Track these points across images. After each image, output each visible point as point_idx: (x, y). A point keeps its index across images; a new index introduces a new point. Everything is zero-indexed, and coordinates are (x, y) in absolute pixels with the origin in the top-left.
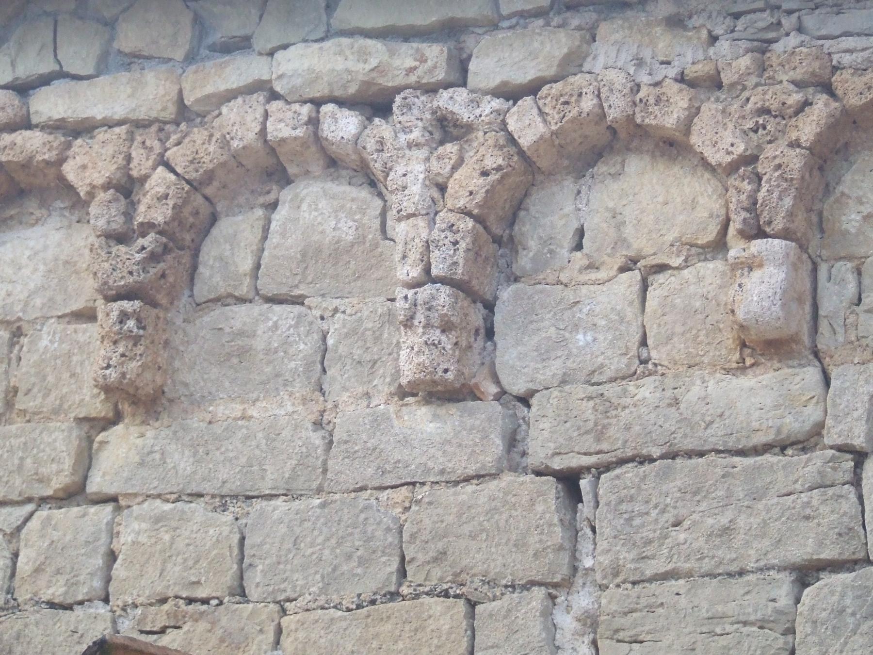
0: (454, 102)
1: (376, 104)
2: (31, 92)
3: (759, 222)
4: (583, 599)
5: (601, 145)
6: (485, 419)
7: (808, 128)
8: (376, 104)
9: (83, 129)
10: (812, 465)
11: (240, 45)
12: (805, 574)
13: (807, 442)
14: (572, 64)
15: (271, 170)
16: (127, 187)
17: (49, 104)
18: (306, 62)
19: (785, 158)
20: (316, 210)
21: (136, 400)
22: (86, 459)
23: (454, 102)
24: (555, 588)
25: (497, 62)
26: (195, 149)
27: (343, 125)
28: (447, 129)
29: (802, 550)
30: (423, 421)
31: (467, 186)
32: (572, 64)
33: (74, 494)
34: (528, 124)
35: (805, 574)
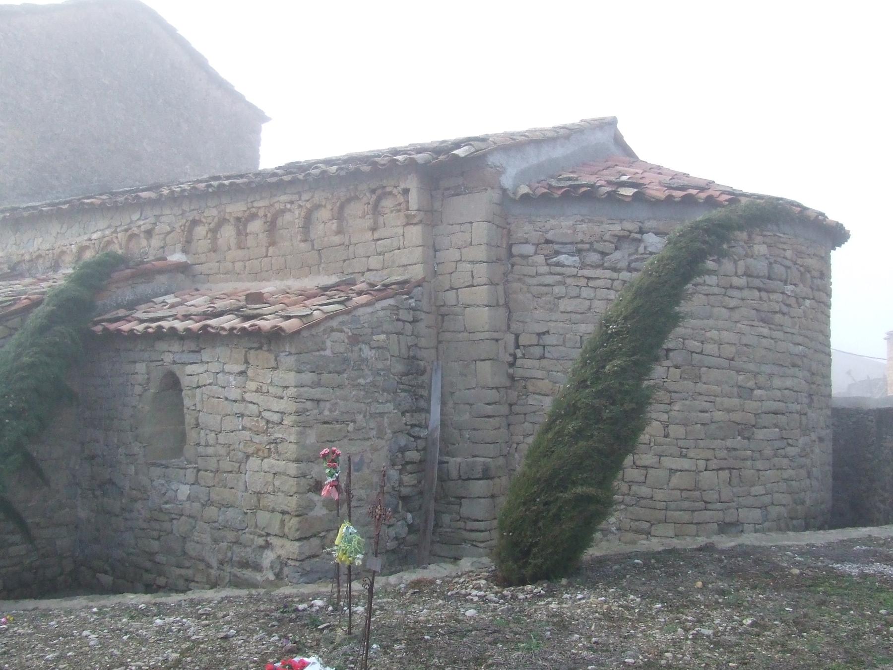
0: (300, 203)
1: (292, 202)
2: (420, 158)
3: (100, 573)
4: (323, 265)
5: (318, 207)
6: (309, 244)
7: (338, 204)
8: (292, 202)
9: (259, 208)
10: (343, 247)
11: (275, 195)
12: (344, 261)
13: (343, 244)
14: (312, 197)
15: (283, 212)
16: (266, 216)
17: (255, 205)
18: (283, 198)
19: (336, 209)
20: (288, 217)
21: (272, 243)
22: (267, 251)
23: (300, 203)
24: (319, 265)
25: (305, 197)
26: (273, 210)
27: (288, 206)
28: (300, 206)
29: (344, 258)
30: (303, 245)
31: (303, 214)
32: (312, 197)
33: (266, 256)
34: (309, 205)
35: (344, 261)
